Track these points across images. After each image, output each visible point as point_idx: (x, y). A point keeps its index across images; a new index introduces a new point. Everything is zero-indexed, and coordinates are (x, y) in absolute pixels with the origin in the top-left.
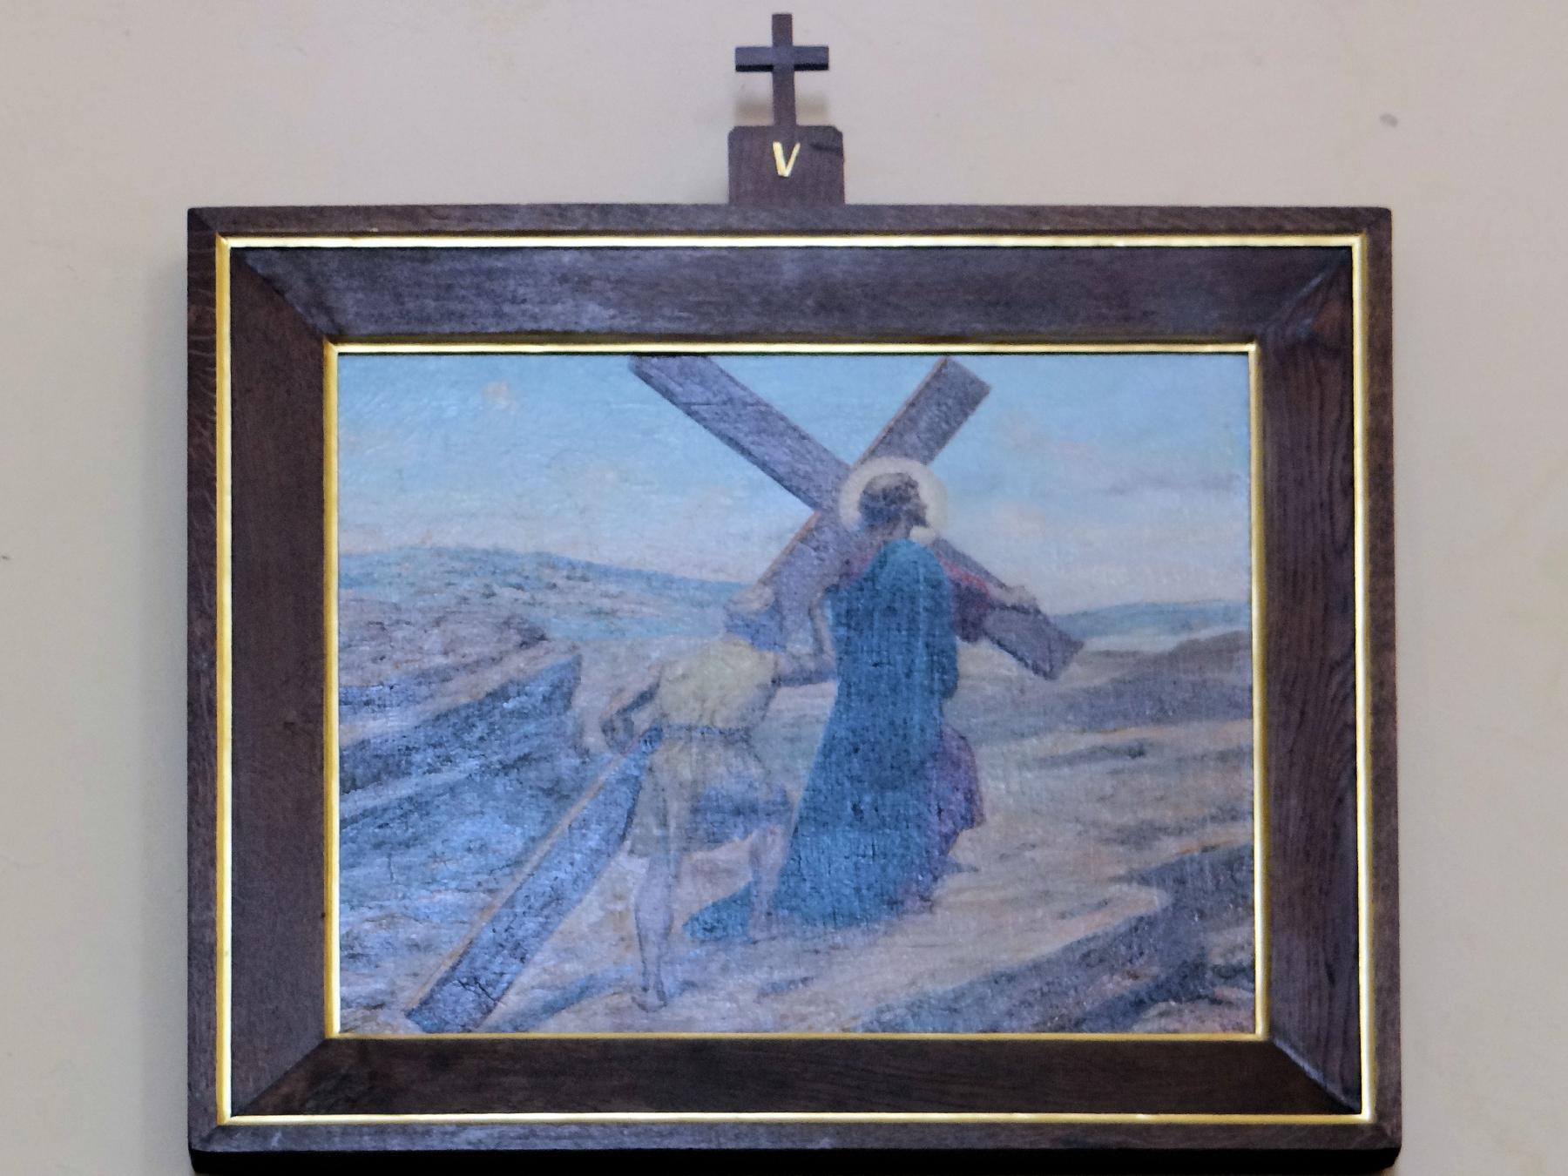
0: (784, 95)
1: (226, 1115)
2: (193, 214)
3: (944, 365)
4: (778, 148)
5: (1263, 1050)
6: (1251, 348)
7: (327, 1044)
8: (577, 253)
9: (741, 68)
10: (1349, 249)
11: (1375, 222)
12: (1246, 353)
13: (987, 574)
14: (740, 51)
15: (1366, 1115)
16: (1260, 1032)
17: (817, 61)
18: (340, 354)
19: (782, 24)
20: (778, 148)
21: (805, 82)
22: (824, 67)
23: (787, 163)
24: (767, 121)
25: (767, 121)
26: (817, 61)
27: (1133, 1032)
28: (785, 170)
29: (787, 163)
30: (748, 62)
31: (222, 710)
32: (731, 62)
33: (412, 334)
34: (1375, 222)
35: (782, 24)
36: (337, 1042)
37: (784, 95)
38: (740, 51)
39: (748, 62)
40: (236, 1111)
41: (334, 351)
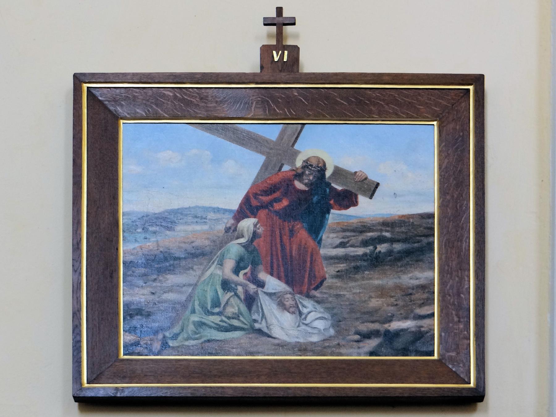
0: (280, 35)
1: (86, 385)
3: (286, 128)
4: (274, 52)
6: (435, 123)
9: (265, 25)
11: (78, 79)
12: (433, 125)
14: (265, 19)
18: (123, 123)
19: (279, 11)
20: (274, 52)
21: (288, 29)
23: (277, 56)
24: (274, 42)
25: (274, 42)
28: (276, 59)
29: (277, 56)
30: (268, 23)
31: (473, 278)
32: (262, 22)
33: (293, 118)
34: (78, 79)
35: (279, 11)
37: (280, 35)
38: (265, 19)
39: (268, 23)
40: (89, 380)
41: (122, 121)
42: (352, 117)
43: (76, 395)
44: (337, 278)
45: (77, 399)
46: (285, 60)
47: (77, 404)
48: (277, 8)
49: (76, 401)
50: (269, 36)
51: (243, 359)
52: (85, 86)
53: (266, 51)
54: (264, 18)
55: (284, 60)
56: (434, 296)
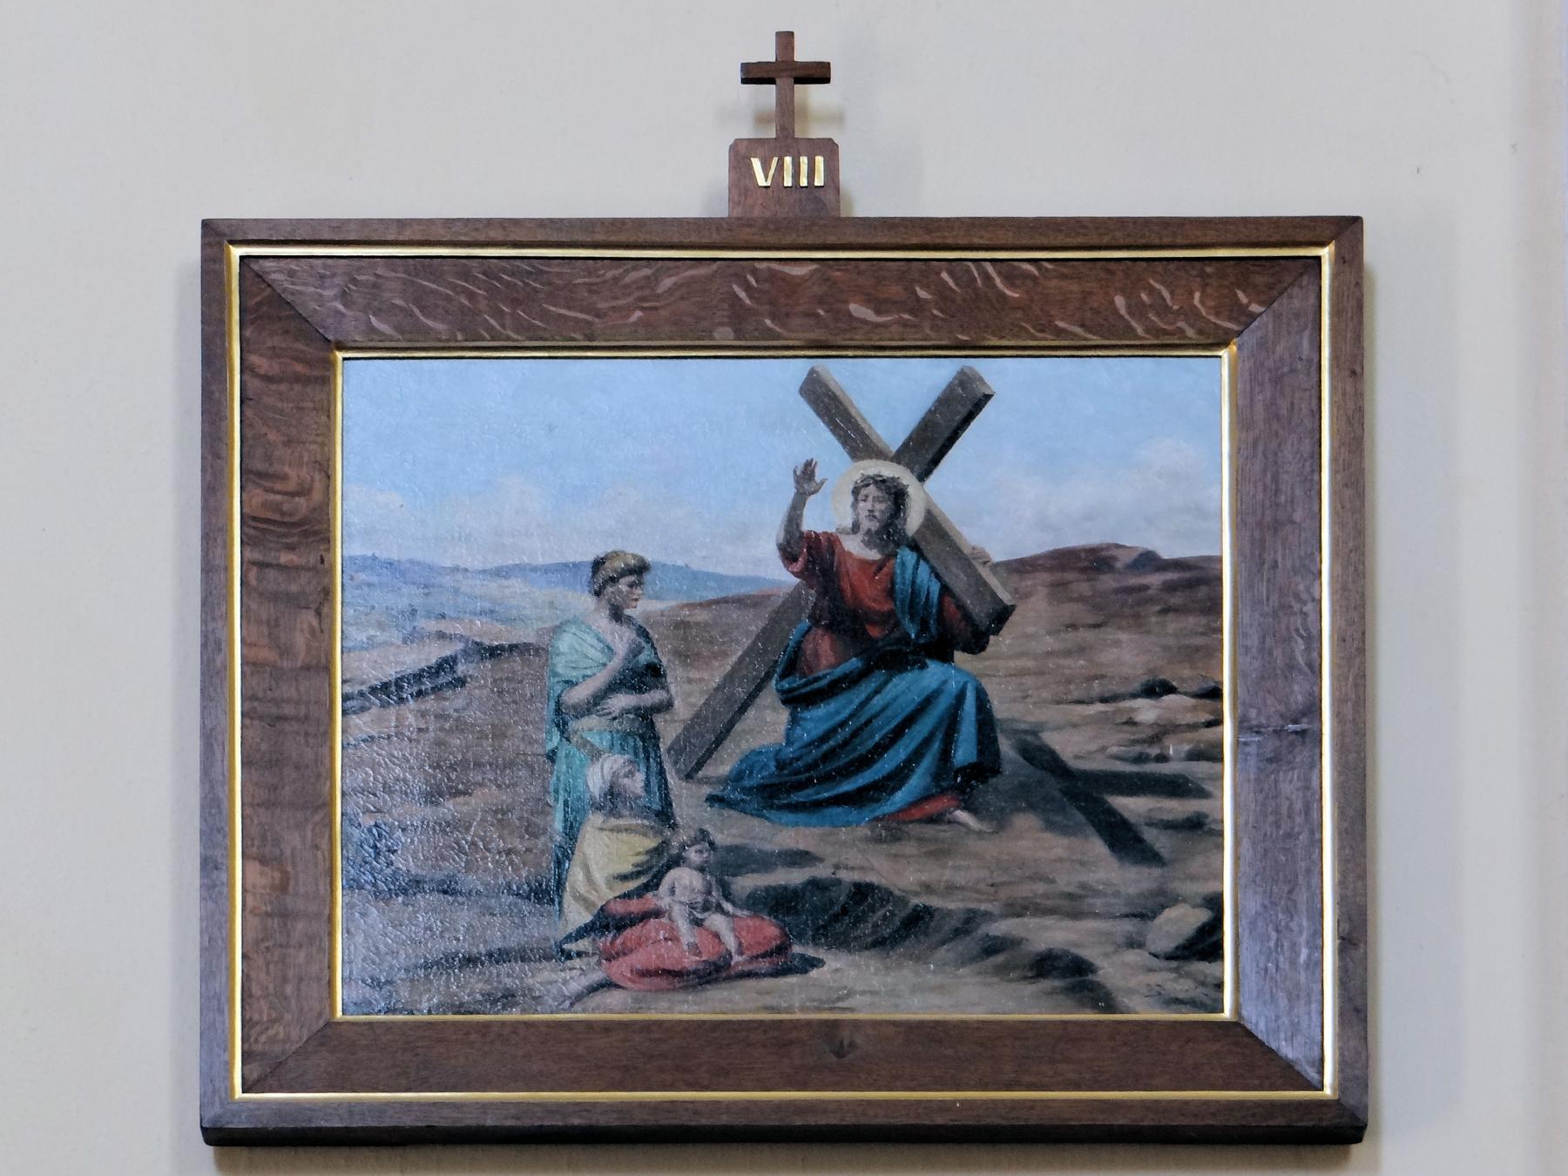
0: (787, 112)
1: (238, 1094)
2: (1357, 221)
4: (756, 164)
5: (1338, 1102)
7: (331, 1024)
8: (1129, 263)
9: (745, 81)
10: (1318, 259)
11: (216, 235)
13: (431, 568)
14: (746, 67)
15: (1328, 1091)
16: (1227, 1014)
17: (818, 74)
18: (345, 359)
19: (786, 40)
20: (756, 164)
21: (813, 95)
22: (826, 80)
26: (818, 74)
27: (511, 1013)
28: (761, 181)
30: (754, 75)
32: (737, 75)
34: (216, 235)
35: (786, 40)
36: (340, 1023)
37: (787, 112)
38: (746, 67)
39: (754, 75)
40: (246, 1087)
42: (778, 337)
43: (206, 1125)
44: (737, 774)
45: (219, 1137)
46: (819, 181)
47: (210, 1150)
48: (779, 34)
49: (208, 1141)
50: (761, 120)
51: (1132, 1101)
52: (237, 252)
53: (740, 155)
54: (829, 64)
55: (816, 184)
56: (1223, 857)
